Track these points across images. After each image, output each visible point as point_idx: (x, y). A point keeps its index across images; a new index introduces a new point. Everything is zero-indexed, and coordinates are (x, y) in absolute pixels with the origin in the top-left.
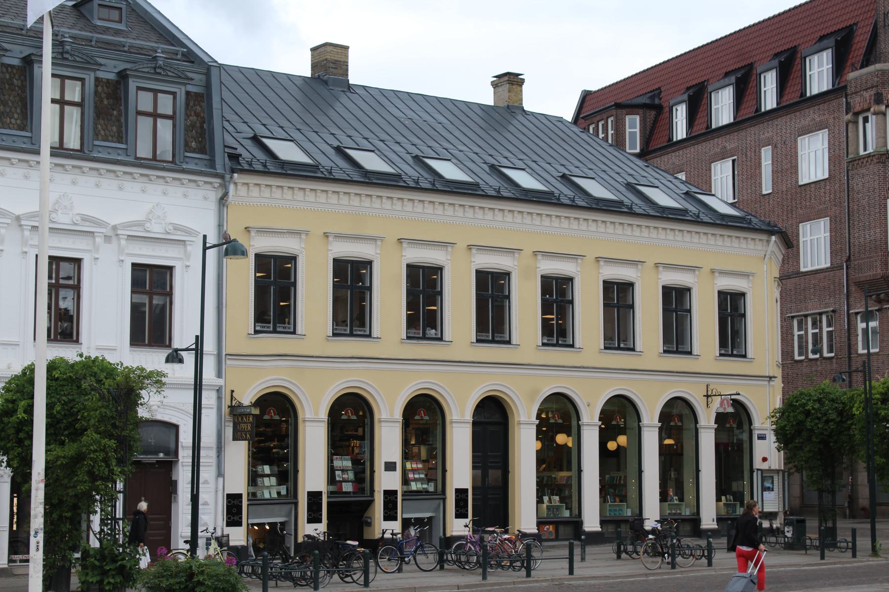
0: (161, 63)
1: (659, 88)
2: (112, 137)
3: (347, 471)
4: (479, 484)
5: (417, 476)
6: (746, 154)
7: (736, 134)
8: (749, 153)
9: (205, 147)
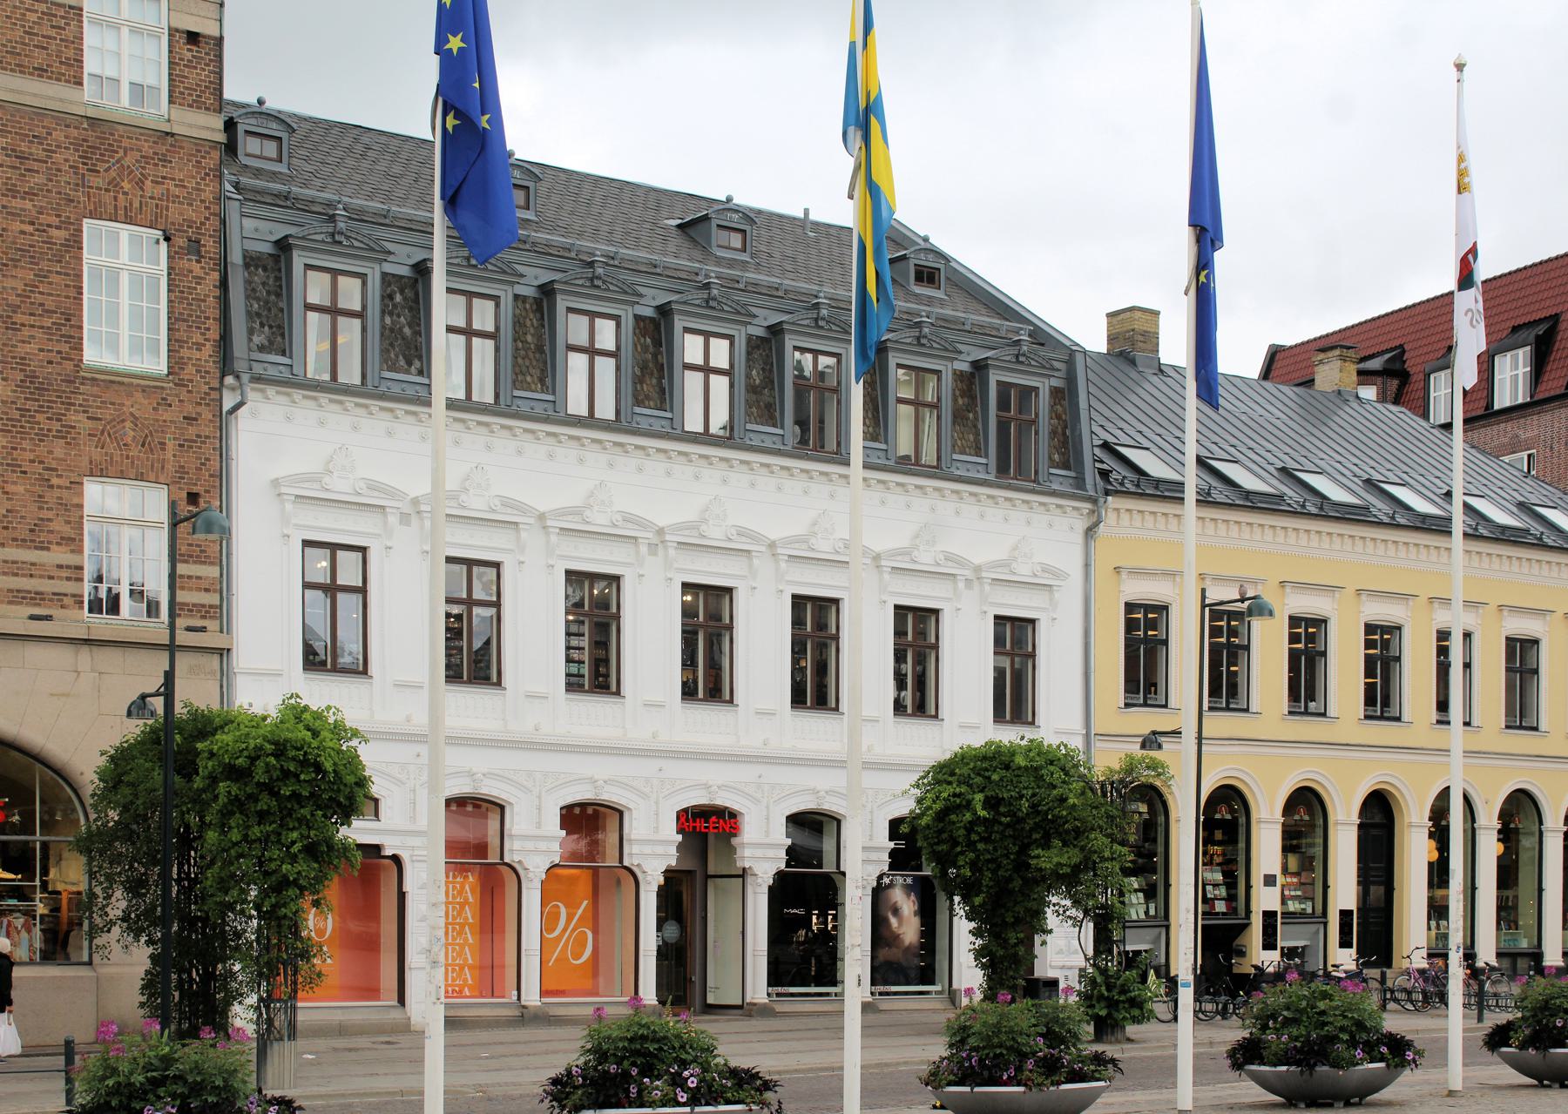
0: (1025, 348)
1: (1401, 346)
2: (970, 448)
3: (1218, 885)
4: (1361, 906)
5: (1293, 893)
6: (1551, 447)
7: (1535, 417)
8: (1556, 446)
9: (1068, 461)
